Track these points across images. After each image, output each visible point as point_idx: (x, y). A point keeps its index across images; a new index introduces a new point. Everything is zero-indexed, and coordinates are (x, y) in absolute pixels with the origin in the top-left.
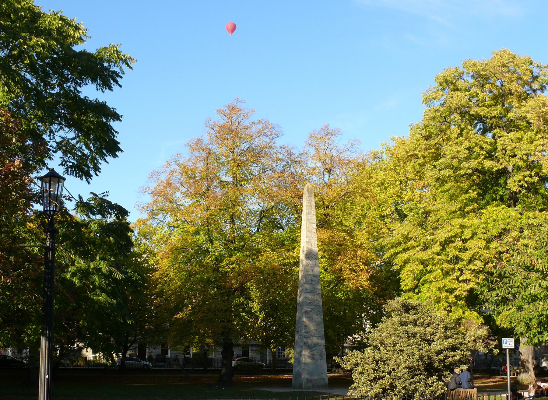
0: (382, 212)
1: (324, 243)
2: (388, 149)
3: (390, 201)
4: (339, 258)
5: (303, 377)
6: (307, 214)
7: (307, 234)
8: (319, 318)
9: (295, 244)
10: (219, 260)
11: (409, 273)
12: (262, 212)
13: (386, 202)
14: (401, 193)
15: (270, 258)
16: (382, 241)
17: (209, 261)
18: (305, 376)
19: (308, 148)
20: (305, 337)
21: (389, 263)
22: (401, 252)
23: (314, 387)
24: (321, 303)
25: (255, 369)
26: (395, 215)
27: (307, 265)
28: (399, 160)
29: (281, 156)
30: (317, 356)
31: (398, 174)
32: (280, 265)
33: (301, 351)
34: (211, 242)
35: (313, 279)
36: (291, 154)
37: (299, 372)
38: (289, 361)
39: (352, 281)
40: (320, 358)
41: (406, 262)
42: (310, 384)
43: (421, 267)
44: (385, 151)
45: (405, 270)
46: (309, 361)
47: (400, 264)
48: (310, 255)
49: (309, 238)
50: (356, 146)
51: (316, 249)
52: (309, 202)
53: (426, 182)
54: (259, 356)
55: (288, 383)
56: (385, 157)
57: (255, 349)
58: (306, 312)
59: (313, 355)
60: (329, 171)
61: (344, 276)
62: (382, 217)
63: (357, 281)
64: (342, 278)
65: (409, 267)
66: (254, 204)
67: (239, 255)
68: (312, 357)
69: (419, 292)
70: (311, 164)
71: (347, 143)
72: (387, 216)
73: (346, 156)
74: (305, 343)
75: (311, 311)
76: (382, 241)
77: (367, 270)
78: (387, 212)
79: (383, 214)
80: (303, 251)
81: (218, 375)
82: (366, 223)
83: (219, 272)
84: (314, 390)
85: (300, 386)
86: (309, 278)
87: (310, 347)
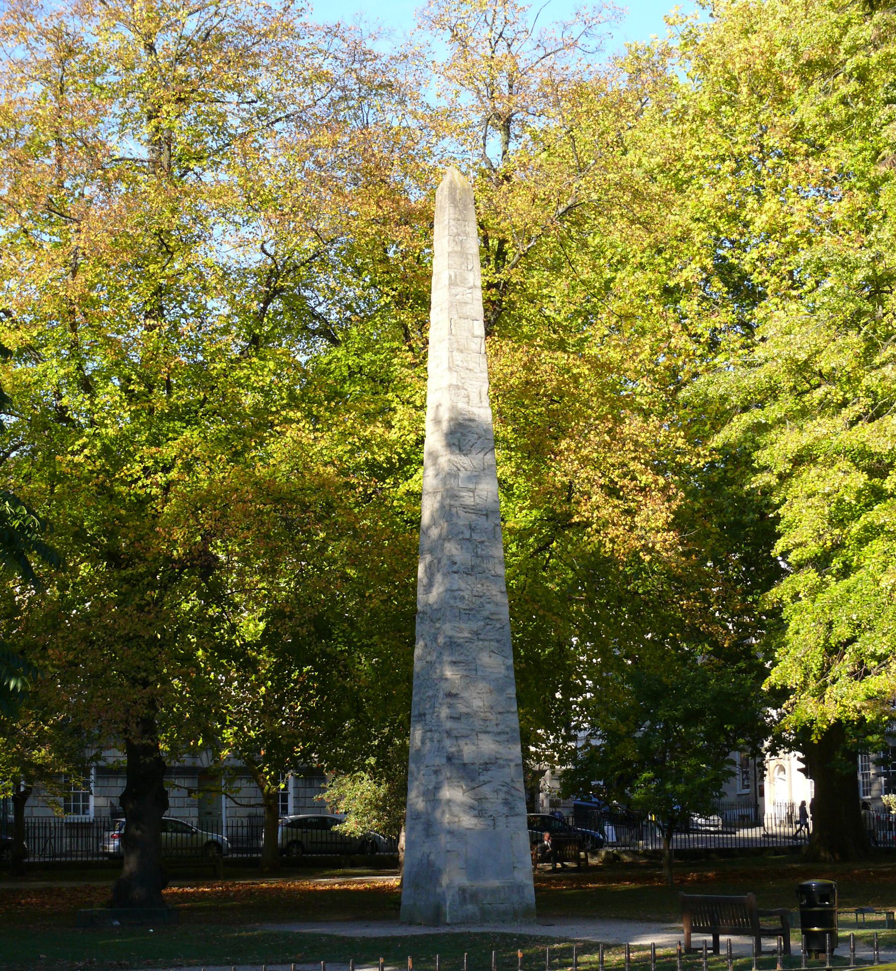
0: (669, 272)
1: (500, 392)
2: (690, 39)
3: (700, 235)
4: (563, 444)
5: (445, 880)
6: (452, 283)
7: (451, 359)
8: (497, 663)
9: (390, 396)
10: (114, 455)
11: (814, 500)
12: (274, 274)
13: (685, 237)
14: (742, 205)
15: (299, 447)
16: (710, 383)
17: (79, 459)
18: (453, 878)
19: (427, 36)
20: (448, 733)
21: (739, 459)
22: (780, 421)
23: (485, 916)
24: (506, 610)
25: (205, 862)
26: (717, 284)
27: (453, 475)
28: (732, 82)
29: (327, 66)
30: (495, 803)
31: (729, 132)
32: (343, 472)
33: (437, 788)
34: (87, 386)
35: (475, 527)
36: (367, 56)
37: (430, 864)
38: (336, 828)
39: (612, 532)
40: (505, 810)
41: (802, 459)
42: (471, 908)
43: (860, 479)
44: (676, 43)
45: (798, 487)
46: (467, 821)
47: (780, 469)
48: (461, 434)
49: (456, 371)
50: (601, 29)
51: (483, 412)
52: (458, 238)
53: (834, 165)
54: (195, 812)
55: (382, 905)
56: (681, 73)
57: (186, 783)
58: (452, 644)
59: (479, 800)
60: (506, 124)
61: (583, 512)
62: (670, 294)
63: (631, 529)
64: (576, 519)
65: (809, 477)
66: (234, 246)
67: (191, 434)
68: (478, 809)
69: (846, 571)
70: (434, 93)
71: (569, 18)
72: (688, 287)
73: (573, 69)
74: (449, 759)
75: (469, 641)
76: (710, 383)
77: (664, 490)
78: (690, 273)
79: (671, 284)
80: (437, 421)
81: (111, 883)
82: (612, 313)
83: (113, 497)
84: (508, 930)
85: (437, 917)
86: (463, 519)
87: (470, 773)
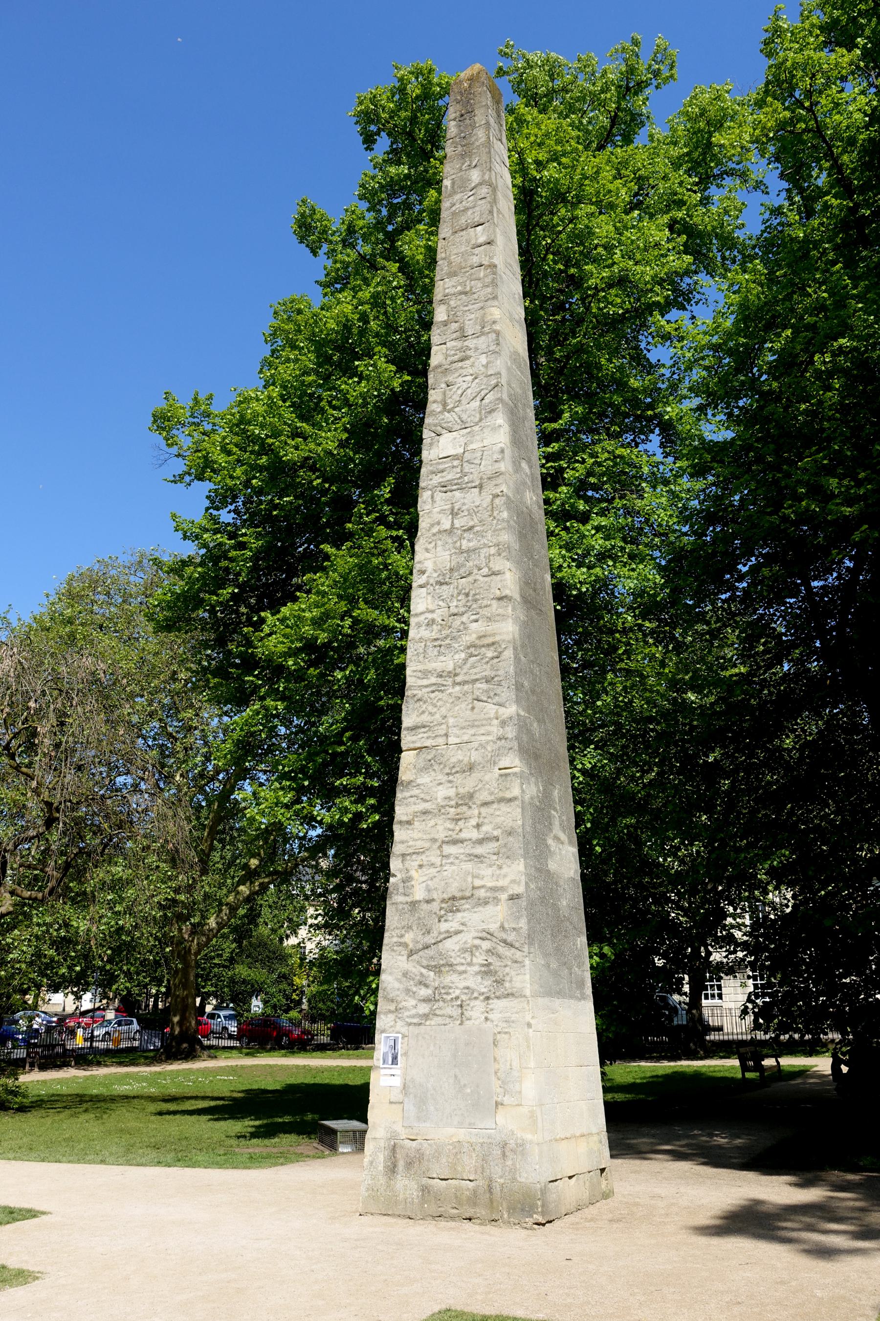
40: (483, 985)
